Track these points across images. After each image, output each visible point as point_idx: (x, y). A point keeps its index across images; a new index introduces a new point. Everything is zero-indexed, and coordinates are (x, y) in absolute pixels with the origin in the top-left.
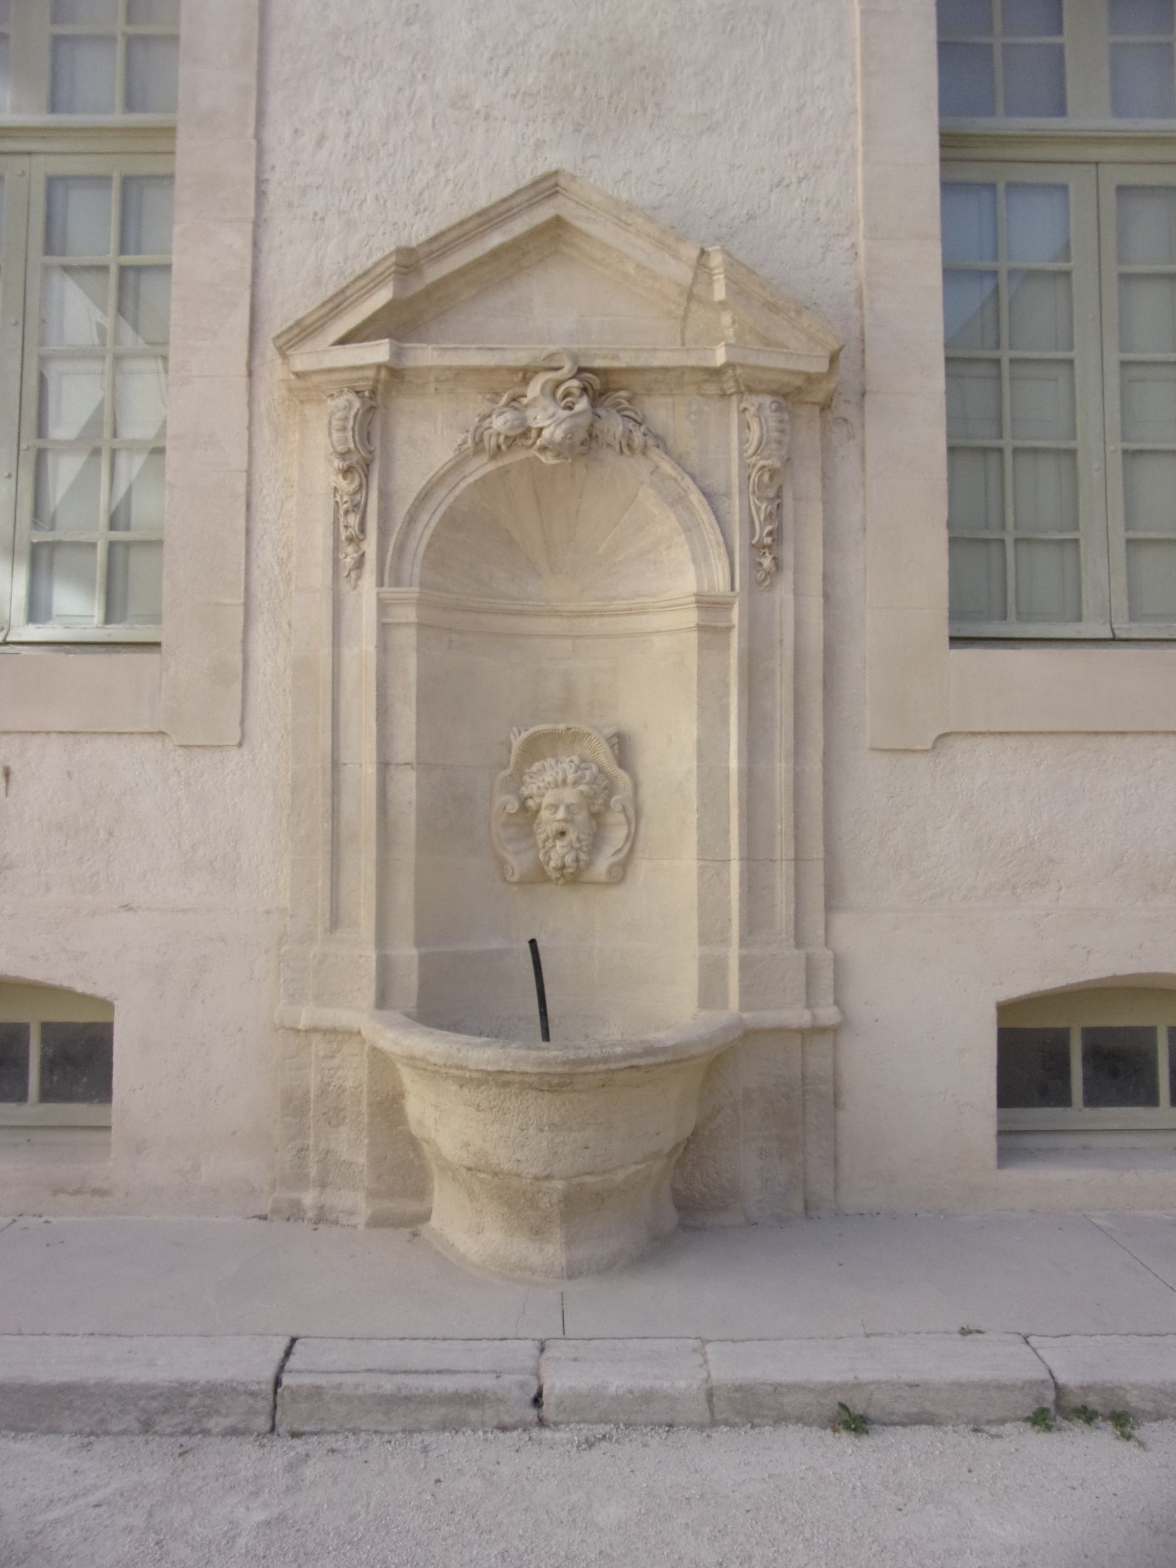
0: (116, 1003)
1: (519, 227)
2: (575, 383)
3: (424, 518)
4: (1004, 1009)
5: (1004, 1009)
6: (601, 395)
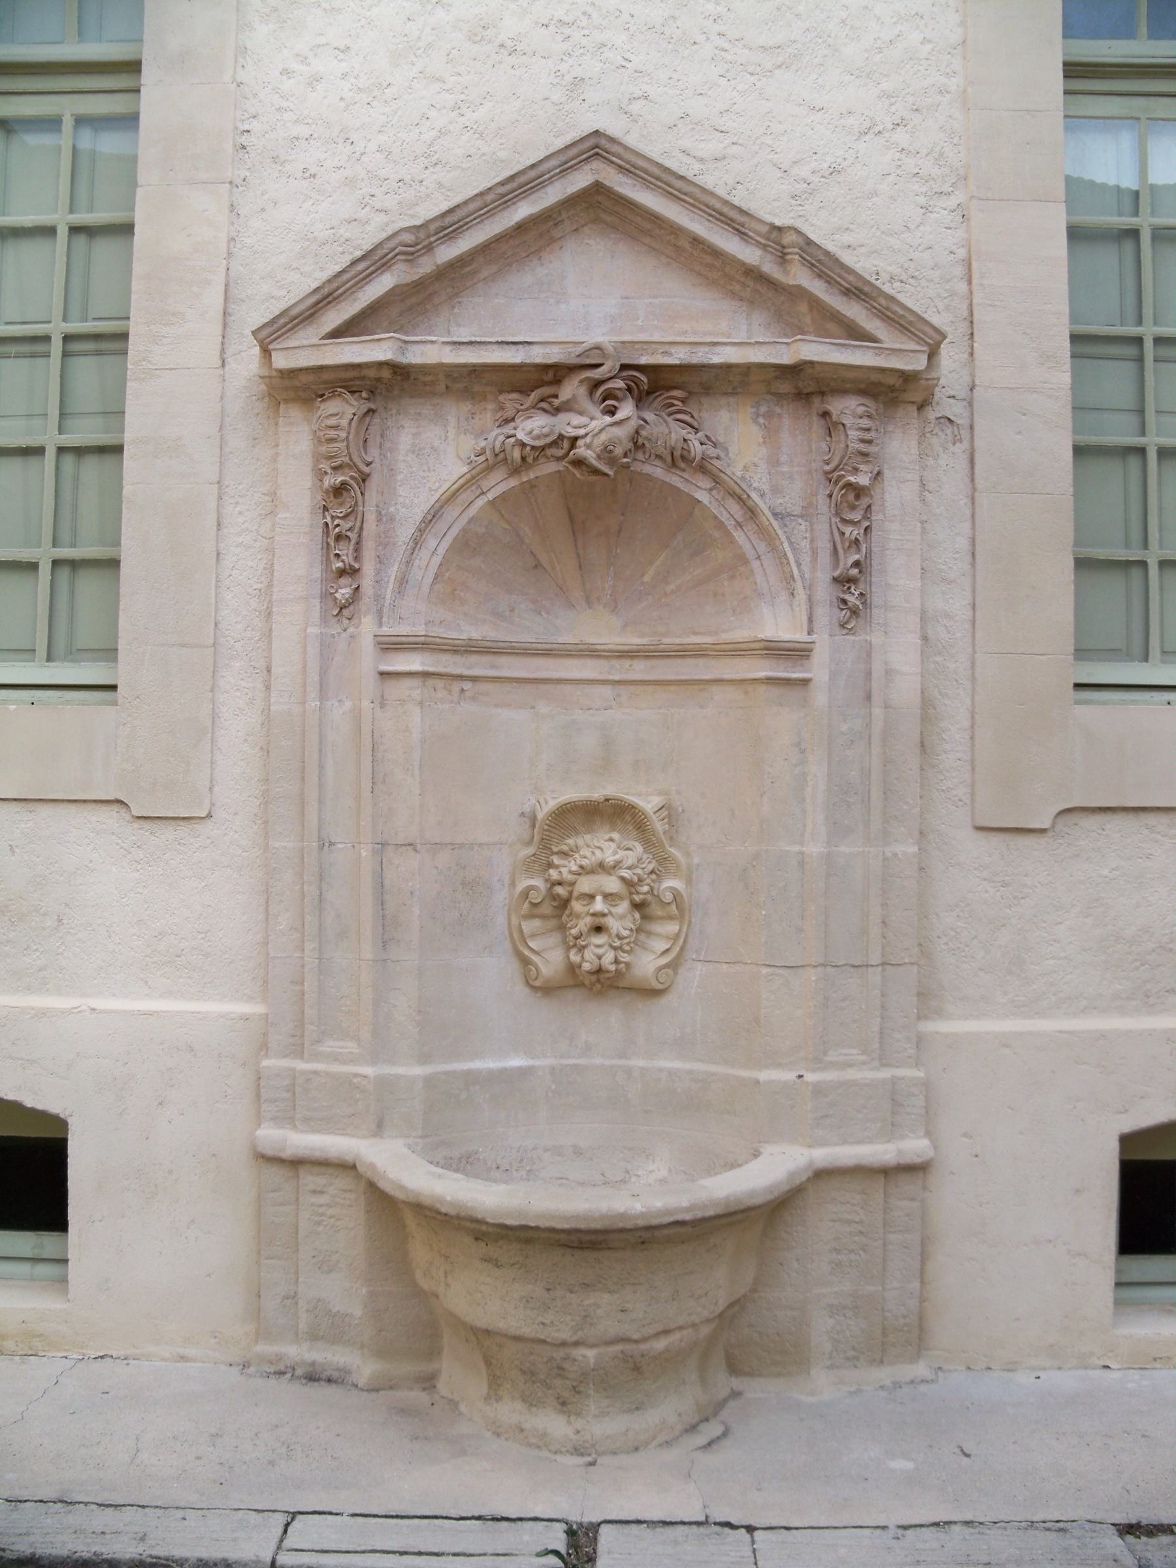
0: (70, 1121)
1: (553, 195)
2: (620, 384)
3: (431, 542)
4: (1127, 1140)
5: (1127, 1140)
6: (649, 393)
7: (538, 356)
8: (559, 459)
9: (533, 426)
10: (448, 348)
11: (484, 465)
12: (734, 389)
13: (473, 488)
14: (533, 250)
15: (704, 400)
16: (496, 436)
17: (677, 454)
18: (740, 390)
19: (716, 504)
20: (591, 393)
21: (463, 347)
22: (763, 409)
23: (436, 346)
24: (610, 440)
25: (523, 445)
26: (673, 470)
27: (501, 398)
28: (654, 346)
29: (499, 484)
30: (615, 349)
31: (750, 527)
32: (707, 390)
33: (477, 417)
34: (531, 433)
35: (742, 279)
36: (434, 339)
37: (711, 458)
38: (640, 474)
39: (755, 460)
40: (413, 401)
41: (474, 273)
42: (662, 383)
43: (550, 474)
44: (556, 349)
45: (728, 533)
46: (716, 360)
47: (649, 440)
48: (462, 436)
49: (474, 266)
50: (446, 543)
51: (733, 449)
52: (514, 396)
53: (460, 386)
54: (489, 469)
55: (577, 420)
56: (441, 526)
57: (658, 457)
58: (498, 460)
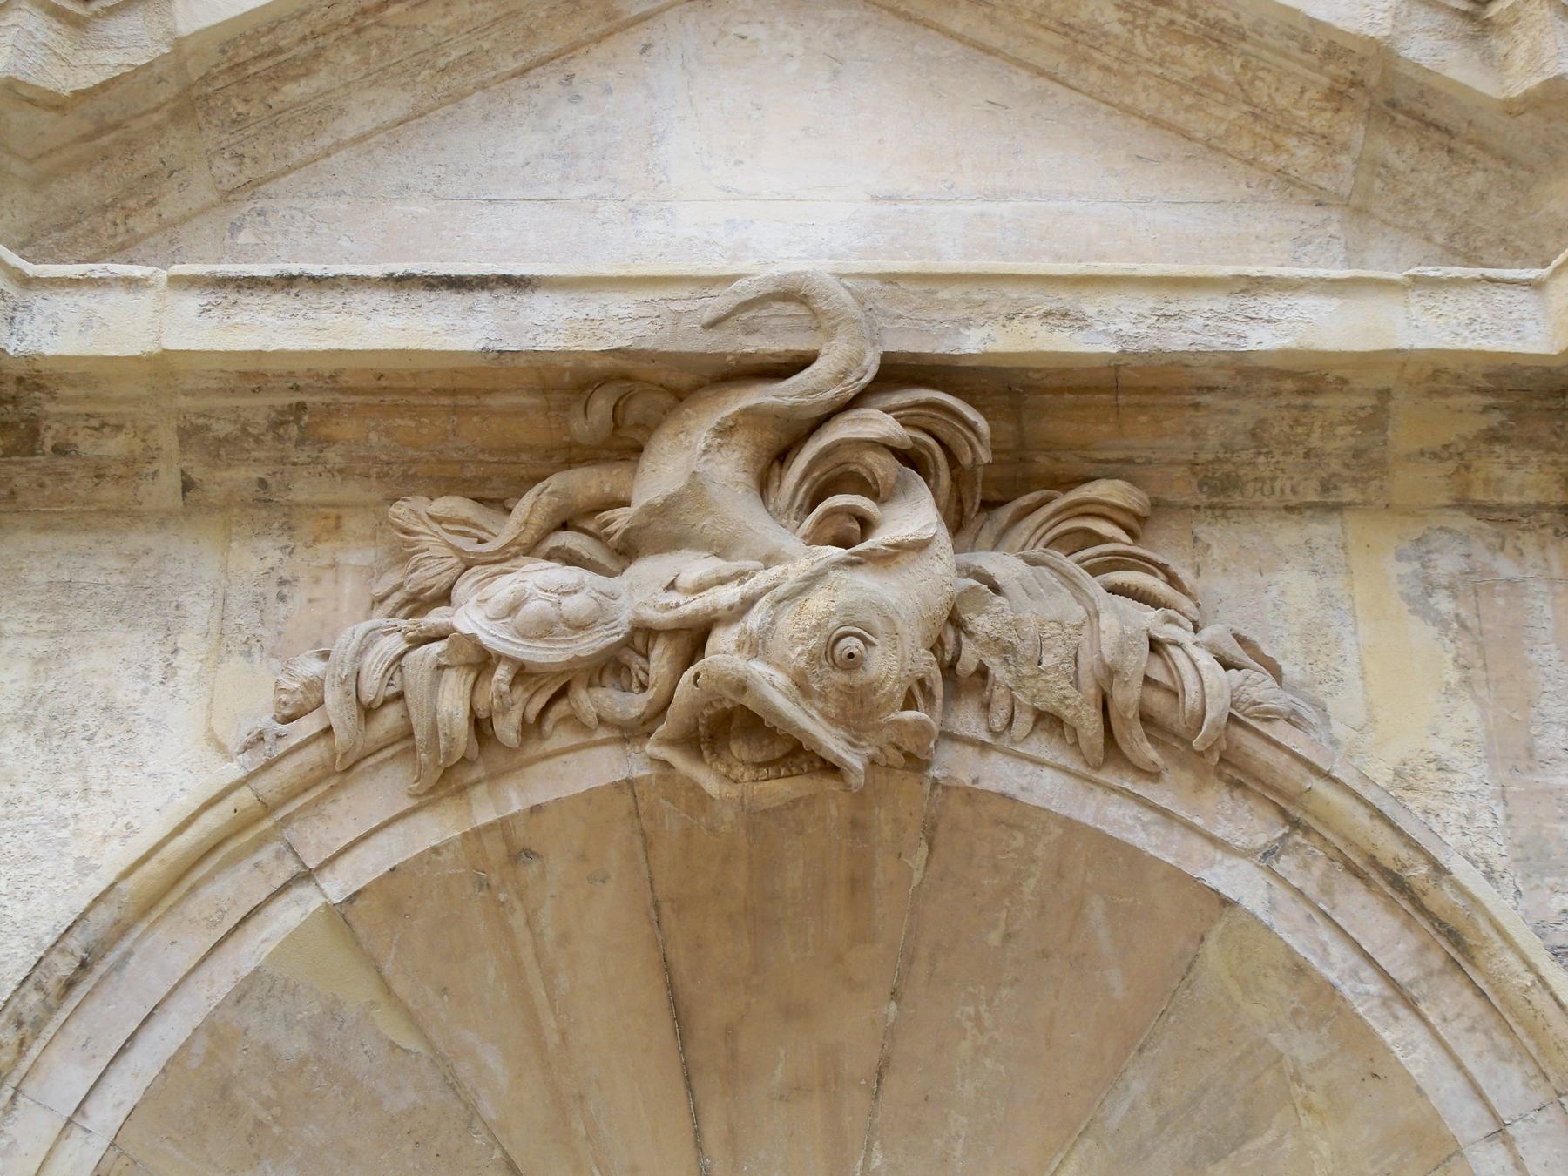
7: (548, 328)
8: (632, 732)
9: (522, 600)
10: (192, 302)
11: (315, 753)
12: (1325, 487)
13: (266, 855)
14: (543, 50)
15: (1213, 533)
16: (370, 642)
17: (1127, 696)
18: (1348, 494)
19: (1298, 911)
20: (764, 485)
21: (254, 300)
22: (1447, 564)
23: (146, 299)
24: (848, 611)
25: (483, 661)
26: (1109, 776)
27: (400, 511)
28: (1013, 293)
29: (377, 834)
30: (861, 300)
31: (1450, 1003)
32: (1221, 492)
33: (299, 596)
34: (514, 608)
35: (1321, 122)
36: (137, 271)
37: (1268, 716)
38: (971, 795)
39: (1441, 748)
40: (45, 541)
41: (323, 110)
42: (1043, 462)
43: (589, 796)
44: (620, 305)
45: (1358, 1037)
46: (1262, 339)
47: (1006, 651)
48: (236, 662)
49: (321, 79)
50: (127, 1087)
51: (1346, 706)
52: (456, 506)
53: (242, 475)
54: (344, 769)
55: (694, 566)
56: (111, 1011)
57: (1049, 721)
58: (374, 733)
